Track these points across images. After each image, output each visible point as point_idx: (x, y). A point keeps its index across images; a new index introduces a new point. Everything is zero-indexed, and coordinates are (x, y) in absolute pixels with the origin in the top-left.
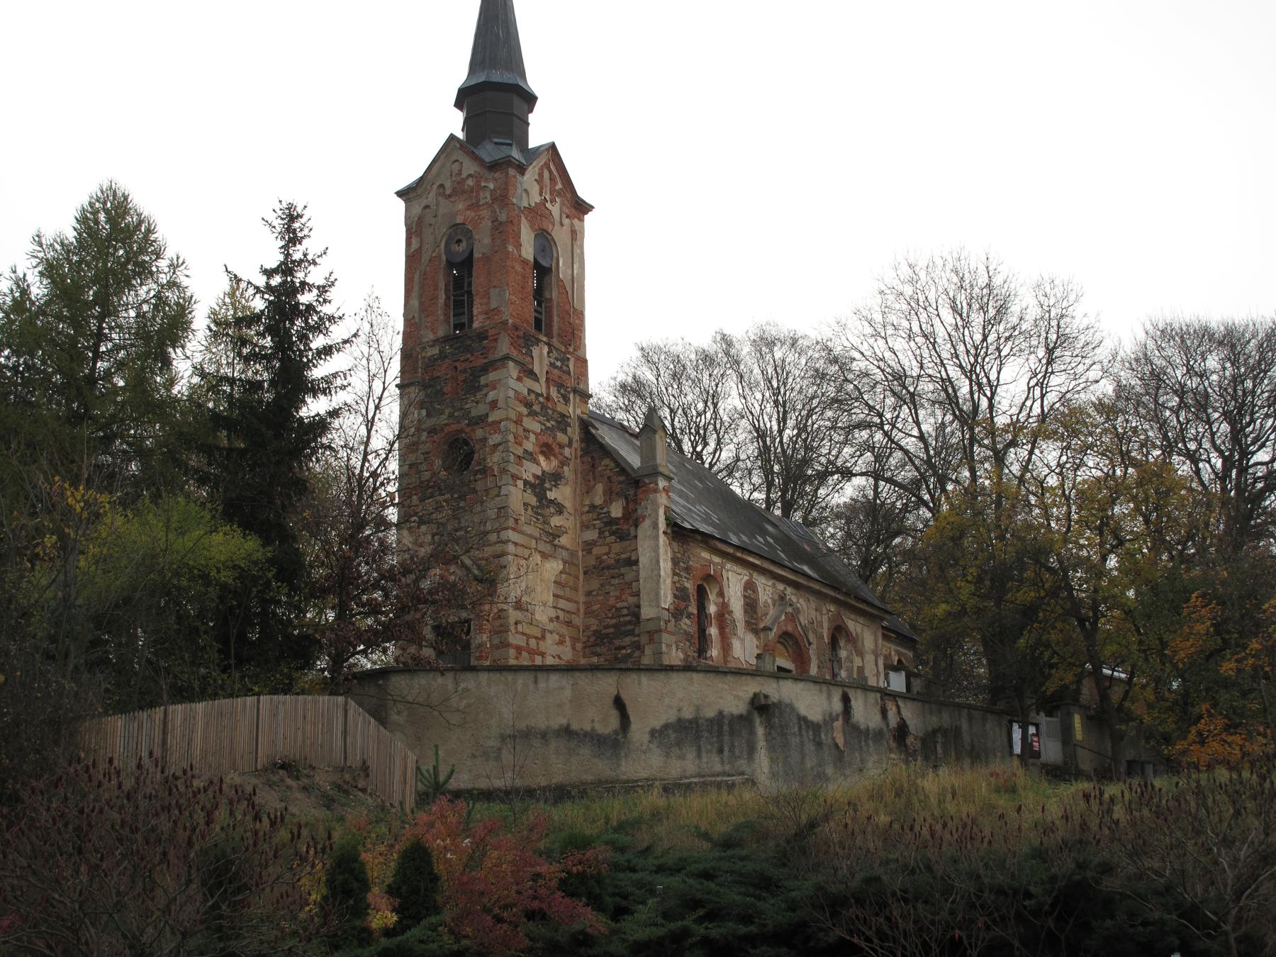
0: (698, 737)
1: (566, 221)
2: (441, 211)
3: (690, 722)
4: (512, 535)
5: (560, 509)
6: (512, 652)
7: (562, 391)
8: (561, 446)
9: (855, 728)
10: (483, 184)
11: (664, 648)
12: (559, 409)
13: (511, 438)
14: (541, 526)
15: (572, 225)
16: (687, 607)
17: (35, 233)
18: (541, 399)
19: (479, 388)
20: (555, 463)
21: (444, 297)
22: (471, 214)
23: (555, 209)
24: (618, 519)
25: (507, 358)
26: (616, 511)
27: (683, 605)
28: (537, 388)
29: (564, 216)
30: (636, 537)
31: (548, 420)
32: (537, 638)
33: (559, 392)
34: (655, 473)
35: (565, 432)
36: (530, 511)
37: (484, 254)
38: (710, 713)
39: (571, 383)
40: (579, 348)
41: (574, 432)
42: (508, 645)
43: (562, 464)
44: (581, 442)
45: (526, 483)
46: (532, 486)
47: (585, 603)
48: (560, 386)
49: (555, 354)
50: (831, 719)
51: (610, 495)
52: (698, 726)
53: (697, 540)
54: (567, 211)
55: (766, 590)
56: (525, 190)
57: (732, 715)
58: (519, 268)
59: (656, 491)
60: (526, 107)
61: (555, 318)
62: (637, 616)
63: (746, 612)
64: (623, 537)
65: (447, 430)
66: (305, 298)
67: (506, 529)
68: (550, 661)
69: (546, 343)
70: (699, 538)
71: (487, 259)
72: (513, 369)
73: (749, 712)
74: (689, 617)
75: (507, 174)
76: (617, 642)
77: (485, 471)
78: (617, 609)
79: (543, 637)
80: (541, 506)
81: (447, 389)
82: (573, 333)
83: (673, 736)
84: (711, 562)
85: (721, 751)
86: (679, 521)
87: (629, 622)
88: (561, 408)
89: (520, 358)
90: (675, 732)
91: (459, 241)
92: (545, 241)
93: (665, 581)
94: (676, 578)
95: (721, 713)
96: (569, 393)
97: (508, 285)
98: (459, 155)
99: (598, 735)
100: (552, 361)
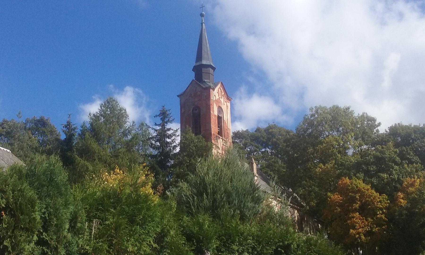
1: (225, 103)
29: (225, 102)
54: (225, 101)
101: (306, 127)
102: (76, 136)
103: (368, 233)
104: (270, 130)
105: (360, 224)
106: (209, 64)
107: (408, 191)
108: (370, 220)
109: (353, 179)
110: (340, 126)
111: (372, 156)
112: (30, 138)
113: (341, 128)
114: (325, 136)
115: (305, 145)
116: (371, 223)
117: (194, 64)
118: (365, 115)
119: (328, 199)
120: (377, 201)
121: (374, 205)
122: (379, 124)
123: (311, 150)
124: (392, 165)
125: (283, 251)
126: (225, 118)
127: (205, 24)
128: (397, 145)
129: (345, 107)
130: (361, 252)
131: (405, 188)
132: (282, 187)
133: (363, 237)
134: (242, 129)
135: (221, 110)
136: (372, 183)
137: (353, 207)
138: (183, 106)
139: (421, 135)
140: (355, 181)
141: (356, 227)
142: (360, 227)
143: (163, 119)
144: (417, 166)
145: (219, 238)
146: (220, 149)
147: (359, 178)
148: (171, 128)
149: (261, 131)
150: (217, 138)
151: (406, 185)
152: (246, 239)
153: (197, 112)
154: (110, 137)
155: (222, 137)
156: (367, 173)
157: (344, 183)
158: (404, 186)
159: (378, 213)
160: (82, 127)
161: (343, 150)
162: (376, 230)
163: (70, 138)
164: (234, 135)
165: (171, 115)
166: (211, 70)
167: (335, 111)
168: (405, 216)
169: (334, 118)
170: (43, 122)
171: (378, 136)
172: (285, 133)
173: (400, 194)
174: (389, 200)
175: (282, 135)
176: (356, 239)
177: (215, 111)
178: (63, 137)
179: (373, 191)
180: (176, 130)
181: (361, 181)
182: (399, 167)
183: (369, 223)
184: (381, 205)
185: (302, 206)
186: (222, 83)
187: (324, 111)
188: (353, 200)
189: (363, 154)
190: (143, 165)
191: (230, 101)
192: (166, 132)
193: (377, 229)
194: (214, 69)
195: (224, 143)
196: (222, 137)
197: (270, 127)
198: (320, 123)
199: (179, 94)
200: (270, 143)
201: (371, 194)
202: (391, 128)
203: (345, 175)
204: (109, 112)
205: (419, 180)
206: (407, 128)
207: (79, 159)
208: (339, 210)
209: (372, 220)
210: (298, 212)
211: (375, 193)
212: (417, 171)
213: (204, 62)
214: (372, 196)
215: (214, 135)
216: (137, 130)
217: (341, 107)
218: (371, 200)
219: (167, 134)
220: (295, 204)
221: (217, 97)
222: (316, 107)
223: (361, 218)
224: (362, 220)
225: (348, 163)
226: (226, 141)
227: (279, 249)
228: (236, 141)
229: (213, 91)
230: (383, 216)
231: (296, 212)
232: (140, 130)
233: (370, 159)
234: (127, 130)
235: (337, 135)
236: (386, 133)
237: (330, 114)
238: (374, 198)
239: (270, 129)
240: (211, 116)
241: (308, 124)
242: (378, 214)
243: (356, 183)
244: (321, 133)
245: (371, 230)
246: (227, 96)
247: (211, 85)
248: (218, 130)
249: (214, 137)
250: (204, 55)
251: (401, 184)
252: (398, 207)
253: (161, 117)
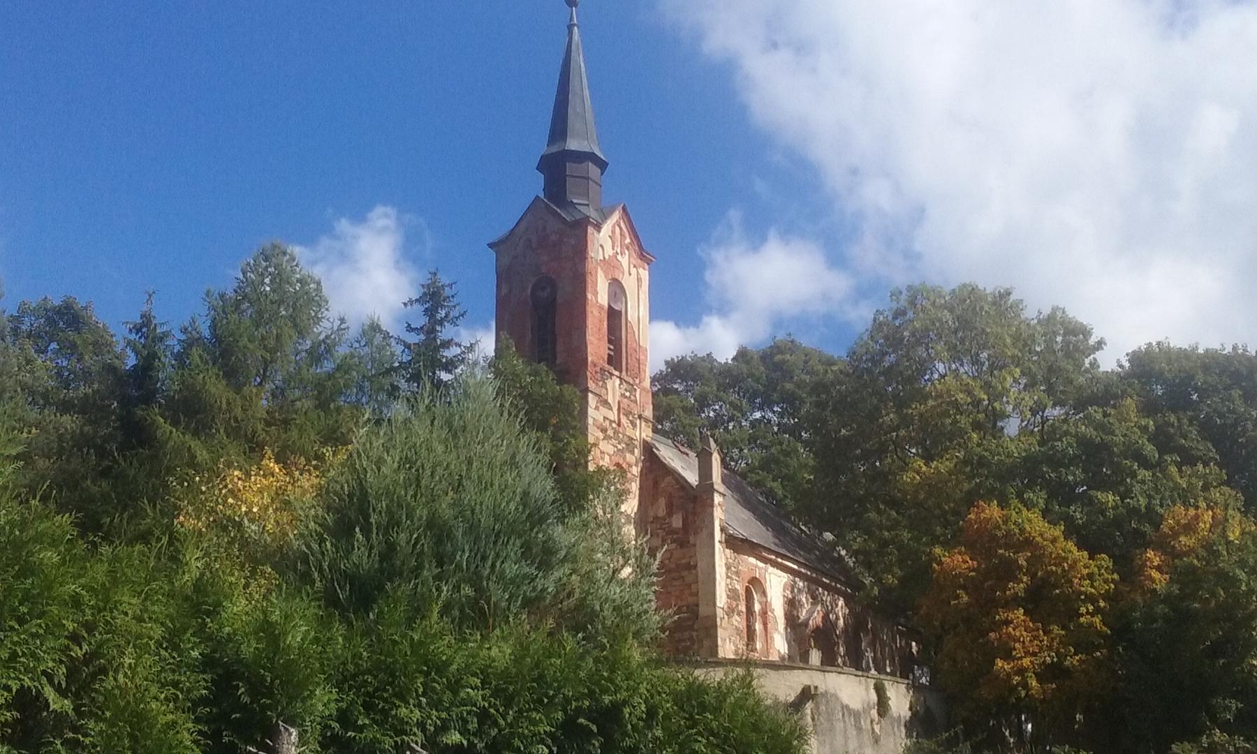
1: (634, 271)
26: (677, 522)
29: (632, 266)
30: (694, 545)
49: (625, 386)
51: (670, 511)
64: (683, 543)
88: (629, 432)
93: (720, 584)
101: (878, 347)
102: (168, 360)
103: (1049, 673)
104: (778, 358)
105: (1027, 643)
106: (587, 150)
107: (1177, 545)
108: (1055, 631)
109: (1012, 507)
110: (984, 347)
111: (1073, 441)
112: (29, 362)
113: (984, 355)
114: (936, 376)
115: (875, 401)
116: (1061, 642)
117: (542, 148)
118: (1059, 314)
119: (934, 565)
120: (1079, 576)
121: (1071, 588)
122: (1100, 345)
123: (890, 417)
124: (1132, 466)
125: (594, 728)
126: (632, 315)
127: (578, 28)
128: (1149, 408)
129: (995, 289)
130: (1030, 726)
131: (1169, 536)
132: (803, 528)
133: (1034, 683)
134: (692, 353)
135: (618, 291)
136: (1069, 520)
137: (1008, 592)
138: (504, 276)
139: (1224, 378)
140: (1017, 513)
141: (1014, 653)
142: (1027, 653)
143: (430, 312)
144: (1208, 471)
145: (342, 682)
146: (611, 409)
147: (1029, 505)
148: (452, 339)
149: (752, 357)
150: (604, 375)
151: (1172, 529)
152: (455, 686)
153: (544, 294)
154: (266, 364)
155: (621, 372)
156: (1061, 494)
157: (985, 518)
158: (1166, 530)
159: (1083, 610)
160: (184, 330)
161: (991, 422)
162: (1073, 661)
163: (146, 369)
164: (669, 370)
165: (455, 301)
166: (593, 170)
167: (966, 300)
168: (1160, 621)
169: (964, 323)
170: (71, 314)
171: (1095, 379)
172: (820, 368)
173: (1150, 554)
174: (1118, 574)
175: (811, 373)
176: (1013, 689)
177: (599, 294)
178: (131, 361)
179: (1071, 545)
180: (469, 345)
181: (1034, 513)
182: (1154, 475)
183: (1053, 639)
184: (1092, 586)
185: (859, 586)
186: (624, 209)
187: (934, 302)
188: (1008, 571)
189: (1048, 435)
190: (347, 450)
191: (648, 264)
192: (439, 352)
193: (1077, 658)
194: (602, 165)
195: (626, 390)
196: (621, 372)
197: (777, 349)
198: (921, 338)
199: (495, 236)
200: (775, 396)
201: (1063, 554)
202: (1135, 357)
203: (989, 495)
204: (268, 289)
205: (1210, 513)
206: (1182, 356)
207: (168, 427)
208: (965, 598)
209: (1063, 632)
210: (846, 605)
211: (1074, 549)
212: (1206, 488)
213: (573, 144)
214: (1065, 559)
215: (595, 366)
216: (356, 345)
217: (985, 289)
218: (1064, 570)
219: (443, 356)
220: (838, 581)
221: (609, 252)
222: (909, 288)
223: (1031, 625)
224: (1034, 630)
225: (999, 457)
226: (632, 385)
227: (582, 720)
228: (675, 386)
229: (595, 233)
230: (1097, 620)
231: (841, 602)
232: (364, 346)
233: (1067, 448)
234: (323, 345)
235: (971, 375)
236: (1120, 370)
237: (951, 310)
238: (1072, 567)
239: (778, 353)
240: (589, 308)
241: (886, 338)
242: (1082, 615)
243: (1020, 521)
244: (924, 367)
245: (1060, 662)
246: (640, 246)
247: (592, 213)
248: (607, 351)
249: (594, 373)
250: (573, 122)
251: (1157, 526)
252: (1143, 594)
253: (426, 306)
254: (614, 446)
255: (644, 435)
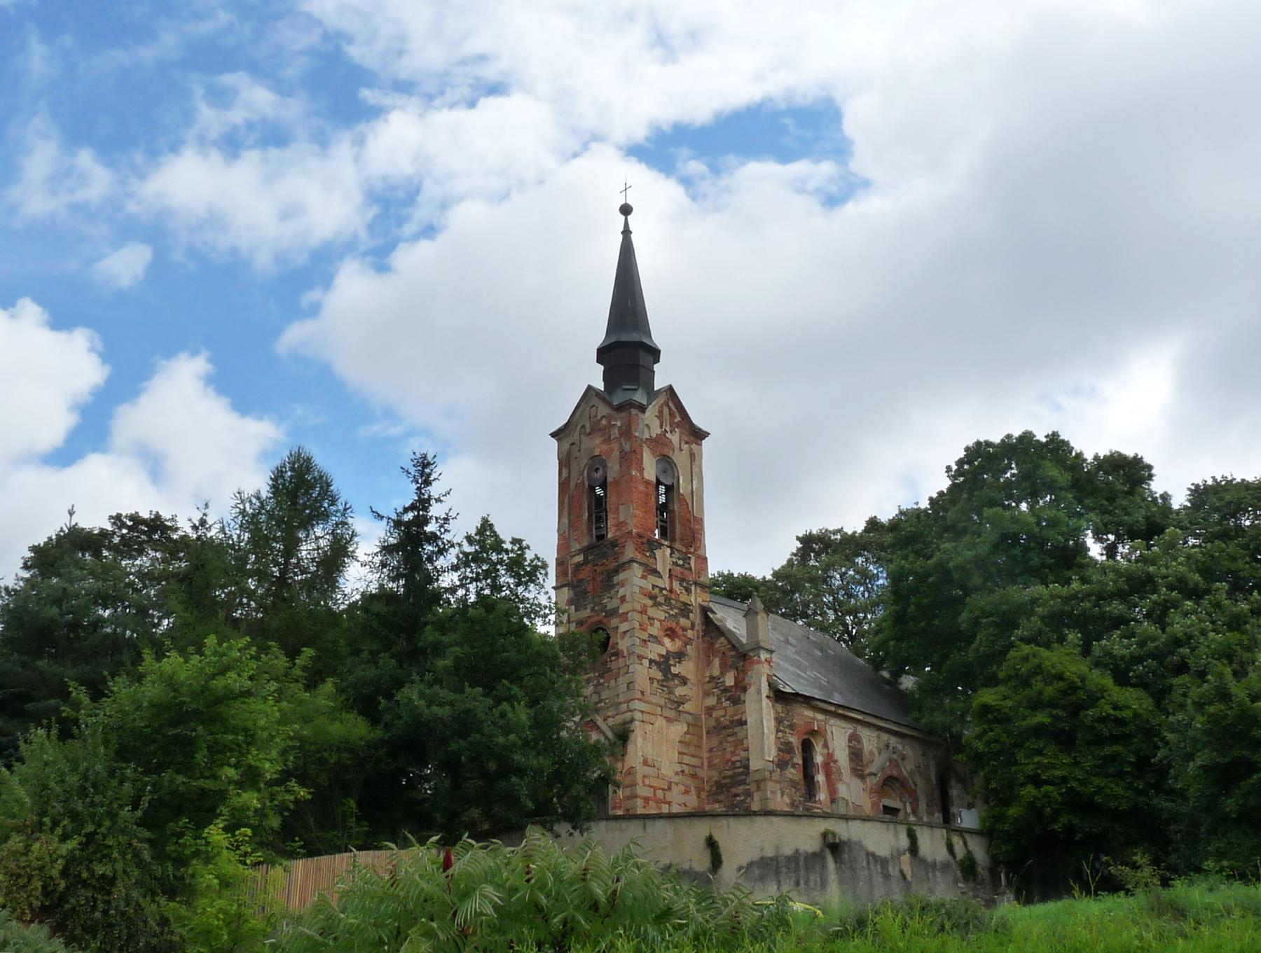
0: (777, 873)
1: (685, 447)
2: (583, 446)
3: (771, 859)
4: (637, 705)
5: (684, 681)
6: (640, 802)
7: (684, 584)
8: (684, 629)
9: (923, 861)
10: (613, 423)
11: (769, 795)
12: (682, 599)
13: (637, 625)
14: (667, 696)
15: (691, 449)
16: (792, 758)
17: (236, 492)
18: (664, 592)
19: (613, 586)
20: (678, 643)
21: (587, 514)
22: (605, 447)
23: (675, 438)
24: (732, 687)
25: (632, 561)
26: (729, 680)
27: (787, 757)
28: (660, 583)
29: (683, 442)
30: (744, 702)
31: (672, 609)
32: (663, 789)
33: (681, 585)
34: (758, 648)
35: (688, 618)
36: (655, 684)
37: (614, 478)
38: (788, 851)
39: (691, 577)
40: (699, 548)
41: (696, 617)
42: (636, 797)
43: (686, 644)
44: (702, 626)
45: (651, 661)
46: (657, 663)
47: (708, 758)
48: (682, 580)
49: (677, 554)
50: (896, 856)
51: (724, 667)
52: (778, 863)
53: (799, 701)
54: (686, 439)
55: (870, 741)
56: (647, 425)
57: (807, 853)
58: (641, 488)
59: (759, 662)
60: (651, 359)
61: (678, 526)
62: (747, 767)
63: (851, 760)
64: (736, 701)
65: (589, 622)
66: (431, 528)
67: (633, 700)
68: (676, 809)
69: (667, 546)
70: (801, 700)
71: (616, 482)
72: (637, 570)
73: (822, 850)
74: (794, 766)
75: (630, 413)
76: (734, 790)
77: (617, 654)
78: (733, 763)
79: (669, 789)
80: (666, 679)
81: (590, 588)
82: (694, 536)
83: (757, 872)
84: (814, 719)
85: (798, 884)
86: (781, 687)
87: (742, 773)
88: (683, 598)
89: (644, 560)
90: (758, 868)
91: (597, 469)
92: (666, 462)
94: (780, 734)
95: (797, 851)
96: (691, 585)
97: (632, 502)
98: (595, 401)
99: (695, 872)
100: (674, 560)
146: (661, 577)
221: (656, 430)
254: (665, 612)
255: (700, 600)
